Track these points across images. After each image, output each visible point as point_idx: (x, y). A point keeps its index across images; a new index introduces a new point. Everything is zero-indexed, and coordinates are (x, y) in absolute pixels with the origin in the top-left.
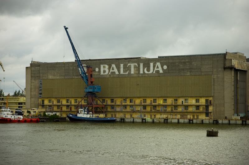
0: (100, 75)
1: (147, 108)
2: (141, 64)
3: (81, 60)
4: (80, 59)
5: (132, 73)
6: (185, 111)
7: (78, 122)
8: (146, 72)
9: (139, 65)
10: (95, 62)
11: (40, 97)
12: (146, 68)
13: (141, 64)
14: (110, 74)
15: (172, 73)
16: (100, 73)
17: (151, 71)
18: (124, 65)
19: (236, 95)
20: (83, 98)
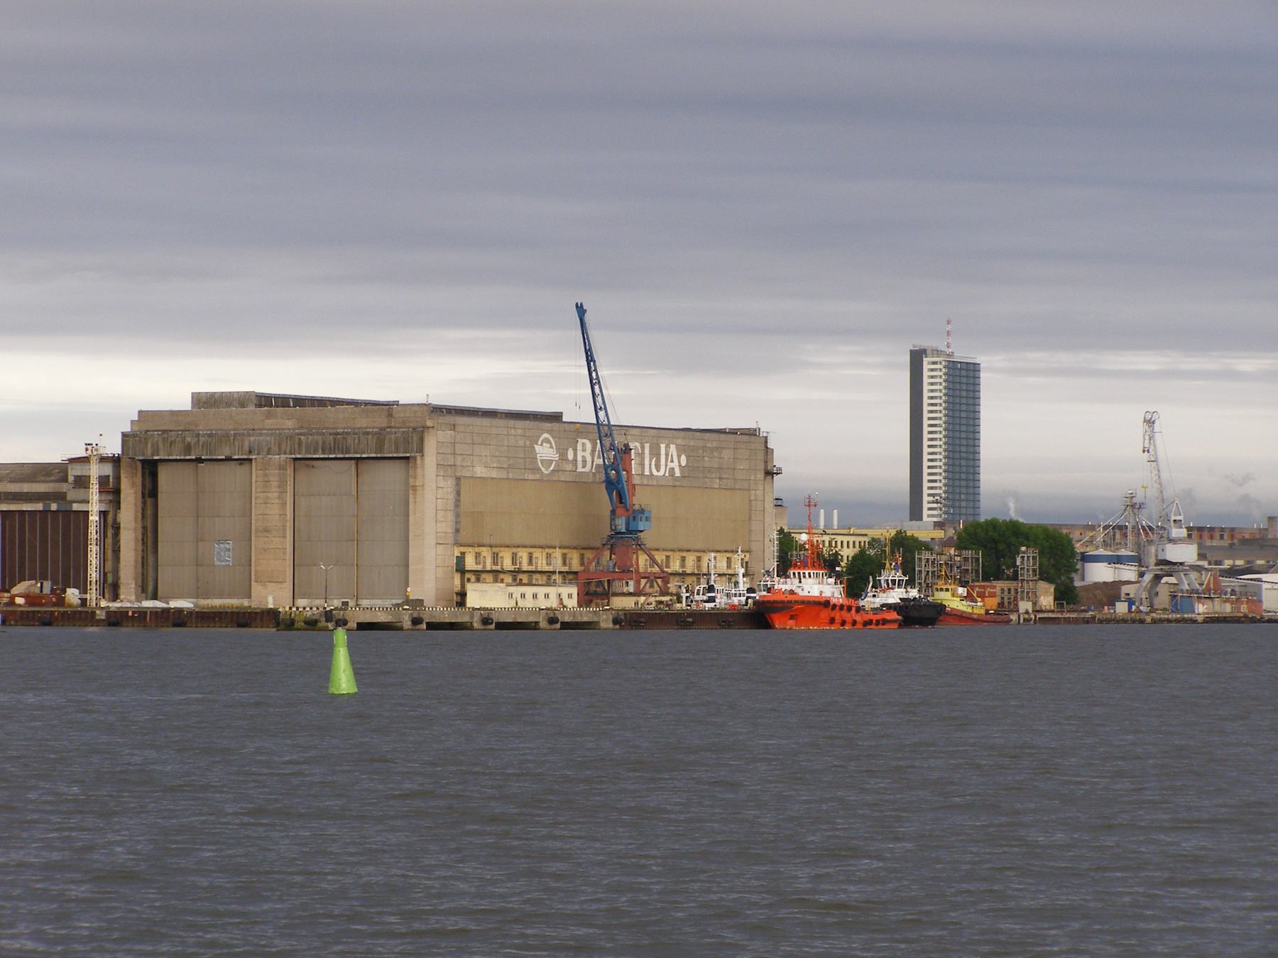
0: (576, 471)
1: (152, 499)
2: (645, 444)
3: (613, 426)
4: (612, 423)
5: (645, 474)
6: (851, 602)
7: (136, 512)
8: (655, 473)
9: (643, 448)
10: (5, 466)
11: (458, 544)
12: (654, 459)
13: (645, 444)
14: (593, 471)
15: (694, 477)
16: (576, 469)
17: (661, 473)
18: (650, 447)
19: (296, 497)
20: (598, 549)
